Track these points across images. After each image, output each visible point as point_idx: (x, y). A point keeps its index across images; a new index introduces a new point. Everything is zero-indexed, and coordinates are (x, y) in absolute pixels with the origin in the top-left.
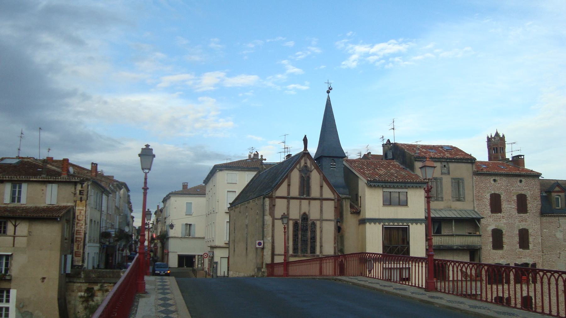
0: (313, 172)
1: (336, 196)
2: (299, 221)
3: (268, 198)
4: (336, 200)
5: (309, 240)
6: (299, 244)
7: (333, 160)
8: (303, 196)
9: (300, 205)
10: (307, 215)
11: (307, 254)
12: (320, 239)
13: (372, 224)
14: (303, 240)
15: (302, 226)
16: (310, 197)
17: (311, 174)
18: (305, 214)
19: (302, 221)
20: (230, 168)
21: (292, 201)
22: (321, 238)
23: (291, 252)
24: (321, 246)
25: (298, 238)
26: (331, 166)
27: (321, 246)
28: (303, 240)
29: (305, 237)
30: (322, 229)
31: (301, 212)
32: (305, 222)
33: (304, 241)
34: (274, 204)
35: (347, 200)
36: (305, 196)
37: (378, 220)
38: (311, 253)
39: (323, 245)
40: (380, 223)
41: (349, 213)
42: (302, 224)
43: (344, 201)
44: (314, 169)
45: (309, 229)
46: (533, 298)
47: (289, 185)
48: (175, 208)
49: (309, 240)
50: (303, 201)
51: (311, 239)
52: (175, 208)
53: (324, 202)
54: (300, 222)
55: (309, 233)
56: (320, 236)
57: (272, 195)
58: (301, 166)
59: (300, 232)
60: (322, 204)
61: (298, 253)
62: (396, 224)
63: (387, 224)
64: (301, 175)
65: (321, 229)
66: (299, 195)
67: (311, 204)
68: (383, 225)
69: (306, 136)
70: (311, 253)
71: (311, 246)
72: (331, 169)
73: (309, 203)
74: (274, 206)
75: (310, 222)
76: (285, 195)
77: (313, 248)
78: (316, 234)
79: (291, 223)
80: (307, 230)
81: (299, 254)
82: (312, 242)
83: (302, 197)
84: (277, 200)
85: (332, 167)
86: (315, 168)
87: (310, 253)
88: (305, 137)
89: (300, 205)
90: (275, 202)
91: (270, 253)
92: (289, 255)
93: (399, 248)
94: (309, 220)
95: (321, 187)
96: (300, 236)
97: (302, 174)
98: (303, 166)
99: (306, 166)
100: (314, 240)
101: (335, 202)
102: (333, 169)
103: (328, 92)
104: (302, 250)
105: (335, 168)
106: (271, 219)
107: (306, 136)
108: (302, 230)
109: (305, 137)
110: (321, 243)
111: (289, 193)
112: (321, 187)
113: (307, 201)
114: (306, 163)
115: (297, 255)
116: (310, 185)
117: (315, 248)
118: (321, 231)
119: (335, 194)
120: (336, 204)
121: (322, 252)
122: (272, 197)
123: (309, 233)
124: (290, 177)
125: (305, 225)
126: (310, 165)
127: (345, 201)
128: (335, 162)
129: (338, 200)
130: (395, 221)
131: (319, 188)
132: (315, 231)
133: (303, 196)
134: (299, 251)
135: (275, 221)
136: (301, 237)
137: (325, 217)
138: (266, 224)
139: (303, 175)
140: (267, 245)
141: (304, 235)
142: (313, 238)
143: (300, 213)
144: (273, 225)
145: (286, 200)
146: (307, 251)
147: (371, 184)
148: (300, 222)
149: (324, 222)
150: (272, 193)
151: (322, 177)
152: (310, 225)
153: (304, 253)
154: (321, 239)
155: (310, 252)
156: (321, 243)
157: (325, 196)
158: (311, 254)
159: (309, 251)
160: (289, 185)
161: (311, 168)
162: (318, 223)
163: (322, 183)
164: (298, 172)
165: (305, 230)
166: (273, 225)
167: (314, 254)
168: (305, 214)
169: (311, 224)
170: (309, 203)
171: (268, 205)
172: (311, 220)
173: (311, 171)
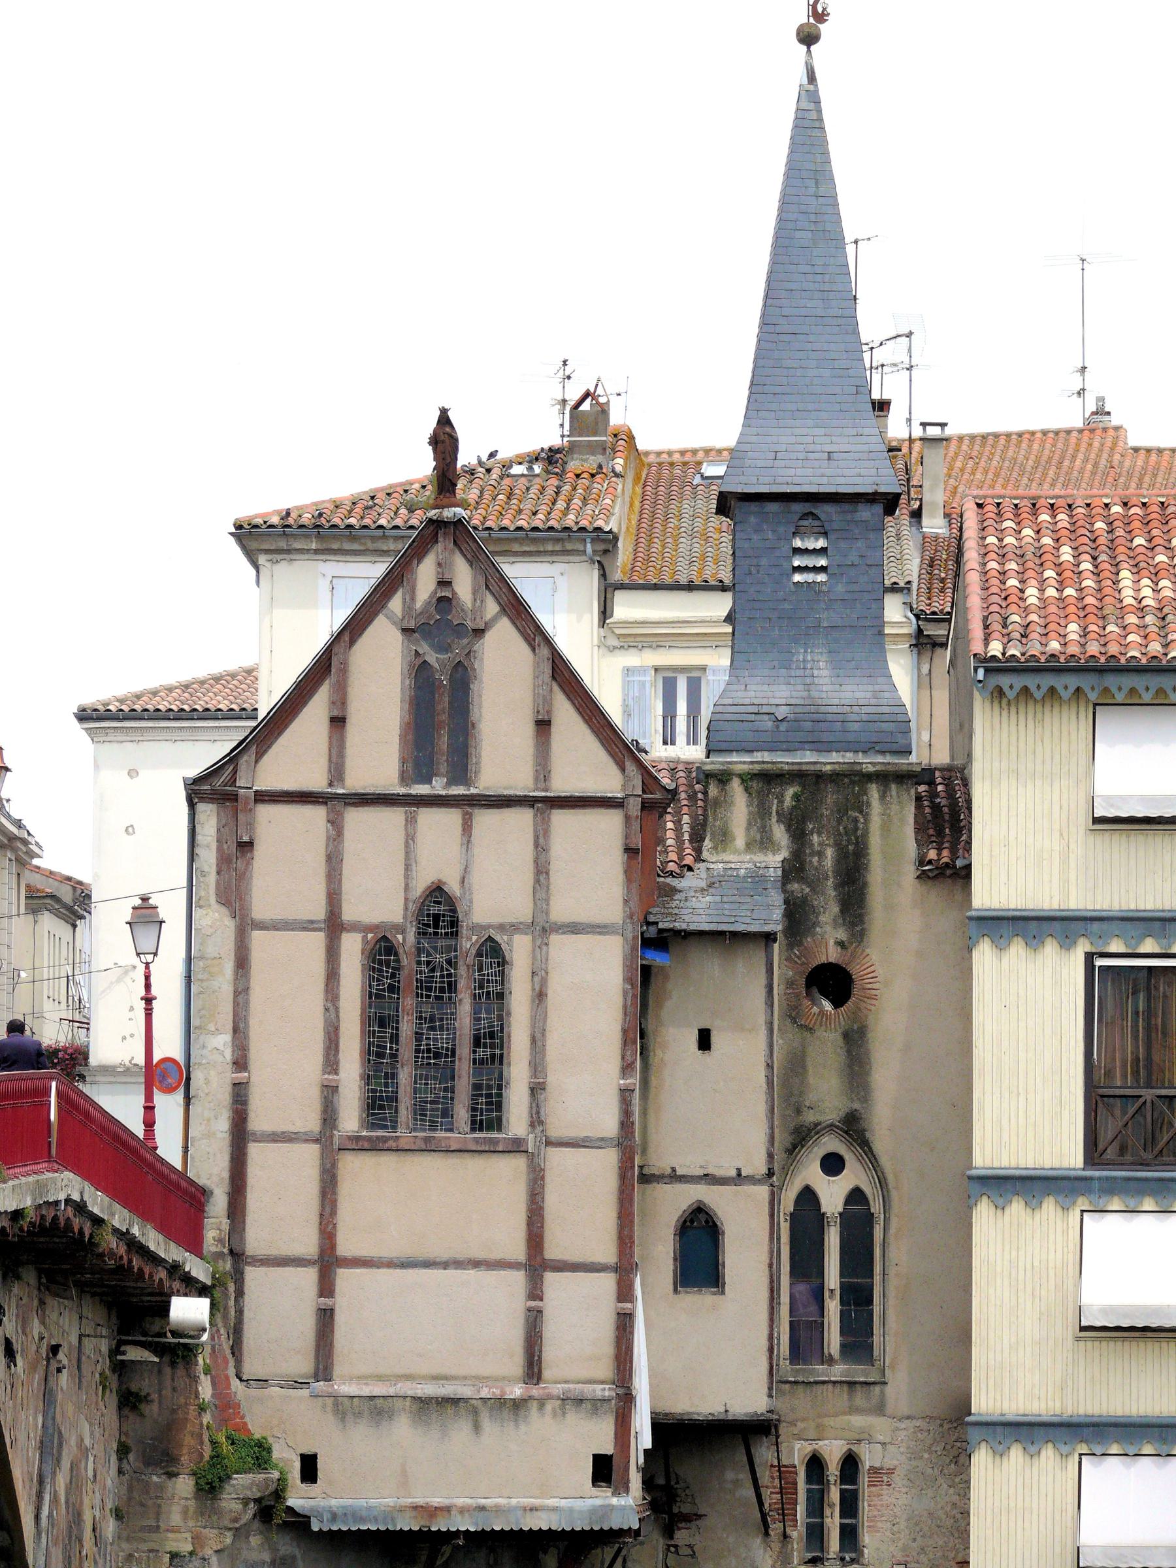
0: (489, 636)
1: (638, 782)
2: (400, 937)
3: (211, 800)
4: (634, 806)
5: (464, 1050)
6: (405, 1076)
7: (815, 517)
8: (430, 782)
9: (410, 839)
10: (450, 901)
11: (451, 1130)
12: (533, 1040)
13: (1017, 948)
14: (429, 1051)
15: (424, 967)
16: (473, 791)
17: (476, 648)
18: (437, 892)
19: (421, 934)
20: (353, 538)
21: (356, 819)
22: (538, 1036)
23: (350, 1120)
24: (536, 1090)
25: (395, 1038)
26: (823, 562)
27: (536, 1090)
28: (429, 1051)
29: (441, 1028)
30: (544, 982)
31: (413, 883)
32: (441, 943)
33: (437, 1055)
34: (246, 838)
35: (893, 786)
36: (438, 786)
37: (1056, 924)
38: (477, 1125)
39: (552, 1079)
40: (1067, 943)
41: (910, 871)
42: (419, 951)
43: (874, 791)
44: (495, 619)
45: (462, 984)
46: (218, 1204)
47: (338, 722)
48: (129, 830)
49: (464, 1050)
50: (428, 817)
51: (477, 1042)
52: (129, 830)
53: (561, 819)
54: (407, 940)
55: (465, 1007)
56: (533, 1026)
57: (233, 781)
58: (413, 599)
59: (408, 1002)
60: (546, 833)
61: (394, 1128)
62: (1149, 946)
63: (1116, 946)
64: (417, 653)
65: (536, 979)
66: (404, 779)
67: (475, 832)
68: (1089, 957)
69: (450, 414)
70: (477, 1125)
71: (477, 1087)
72: (797, 578)
73: (467, 828)
74: (246, 846)
75: (468, 943)
76: (316, 781)
77: (489, 1096)
78: (509, 1014)
79: (352, 948)
80: (452, 987)
81: (402, 1132)
82: (482, 1062)
83: (422, 789)
84: (266, 813)
85: (799, 569)
86: (503, 610)
87: (468, 1129)
88: (444, 420)
89: (410, 839)
90: (251, 825)
91: (223, 1125)
92: (336, 1141)
93: (1145, 1102)
94: (464, 931)
95: (543, 725)
96: (407, 1028)
97: (423, 647)
98: (428, 603)
99: (444, 602)
100: (492, 1046)
101: (627, 818)
102: (810, 577)
103: (808, 38)
104: (419, 1112)
105: (823, 569)
106: (227, 926)
107: (444, 413)
108: (424, 988)
109: (444, 420)
110: (537, 1065)
111: (337, 771)
112: (543, 725)
113: (451, 818)
114: (444, 583)
115: (385, 1140)
116: (474, 715)
117: (500, 1095)
118: (540, 996)
119: (630, 766)
120: (636, 826)
121: (541, 1123)
122: (234, 797)
123: (465, 1007)
124: (344, 671)
125: (439, 958)
126: (475, 592)
127: (883, 797)
128: (825, 534)
129: (646, 806)
130: (1075, 925)
131: (528, 729)
132: (501, 996)
133: (430, 782)
134: (404, 1112)
135: (256, 935)
136: (418, 1036)
137: (562, 909)
138: (202, 958)
139: (432, 658)
140: (207, 1081)
141: (432, 1019)
142: (492, 1035)
143: (407, 888)
144: (242, 963)
145: (318, 814)
146: (447, 1113)
147: (1005, 681)
148: (411, 937)
149: (555, 939)
150: (235, 772)
151: (548, 670)
152: (470, 960)
153: (433, 1128)
154: (537, 1041)
155: (473, 1122)
156: (537, 1065)
157: (561, 786)
158: (473, 1130)
159: (462, 1114)
160: (338, 722)
161: (478, 610)
162: (519, 950)
163: (548, 702)
164: (398, 636)
165: (442, 990)
166: (242, 963)
167: (495, 1135)
168: (437, 892)
169: (479, 954)
170: (467, 828)
171: (214, 845)
172: (474, 928)
173: (479, 633)
